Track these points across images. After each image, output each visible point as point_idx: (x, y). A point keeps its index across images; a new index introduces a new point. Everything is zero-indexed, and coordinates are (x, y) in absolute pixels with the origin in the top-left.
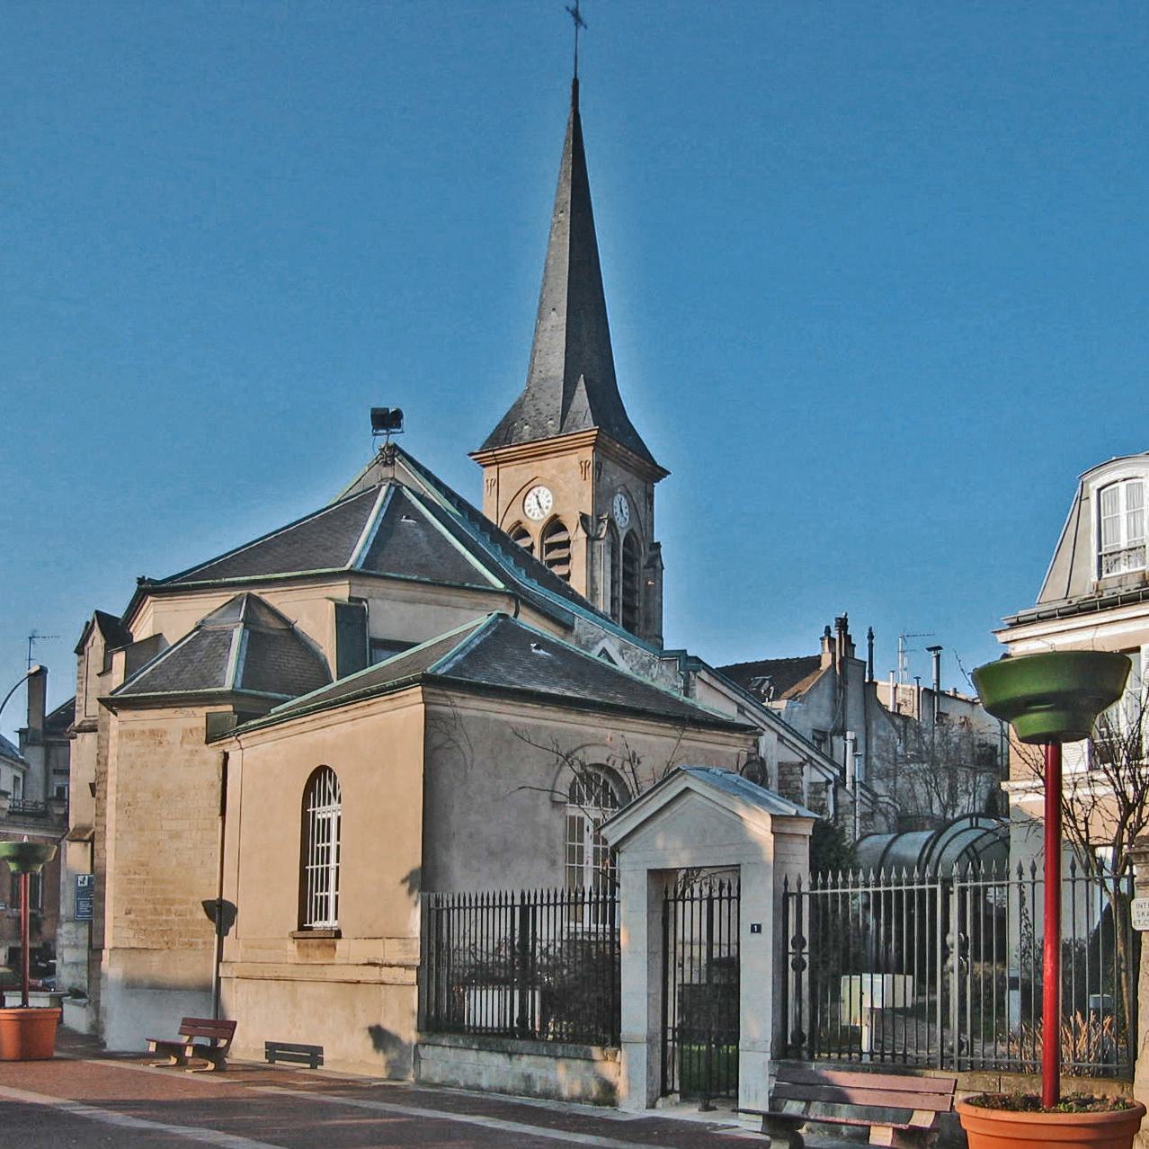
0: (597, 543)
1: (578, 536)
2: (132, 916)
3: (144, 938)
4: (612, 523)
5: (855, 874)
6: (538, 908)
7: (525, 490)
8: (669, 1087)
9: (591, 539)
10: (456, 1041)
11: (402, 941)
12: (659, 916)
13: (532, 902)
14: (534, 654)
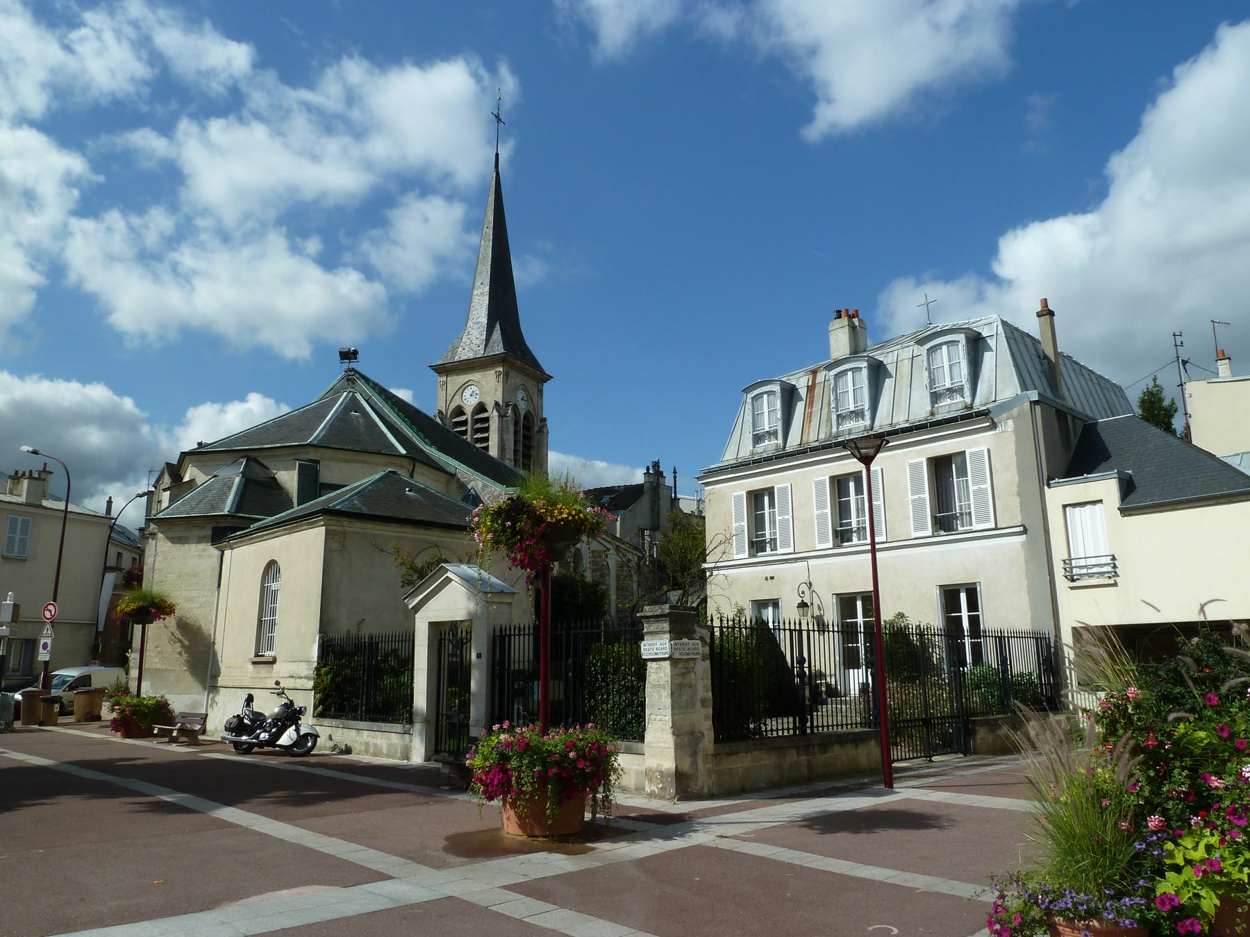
1: (494, 416)
4: (515, 408)
7: (464, 387)
9: (501, 416)
12: (436, 648)
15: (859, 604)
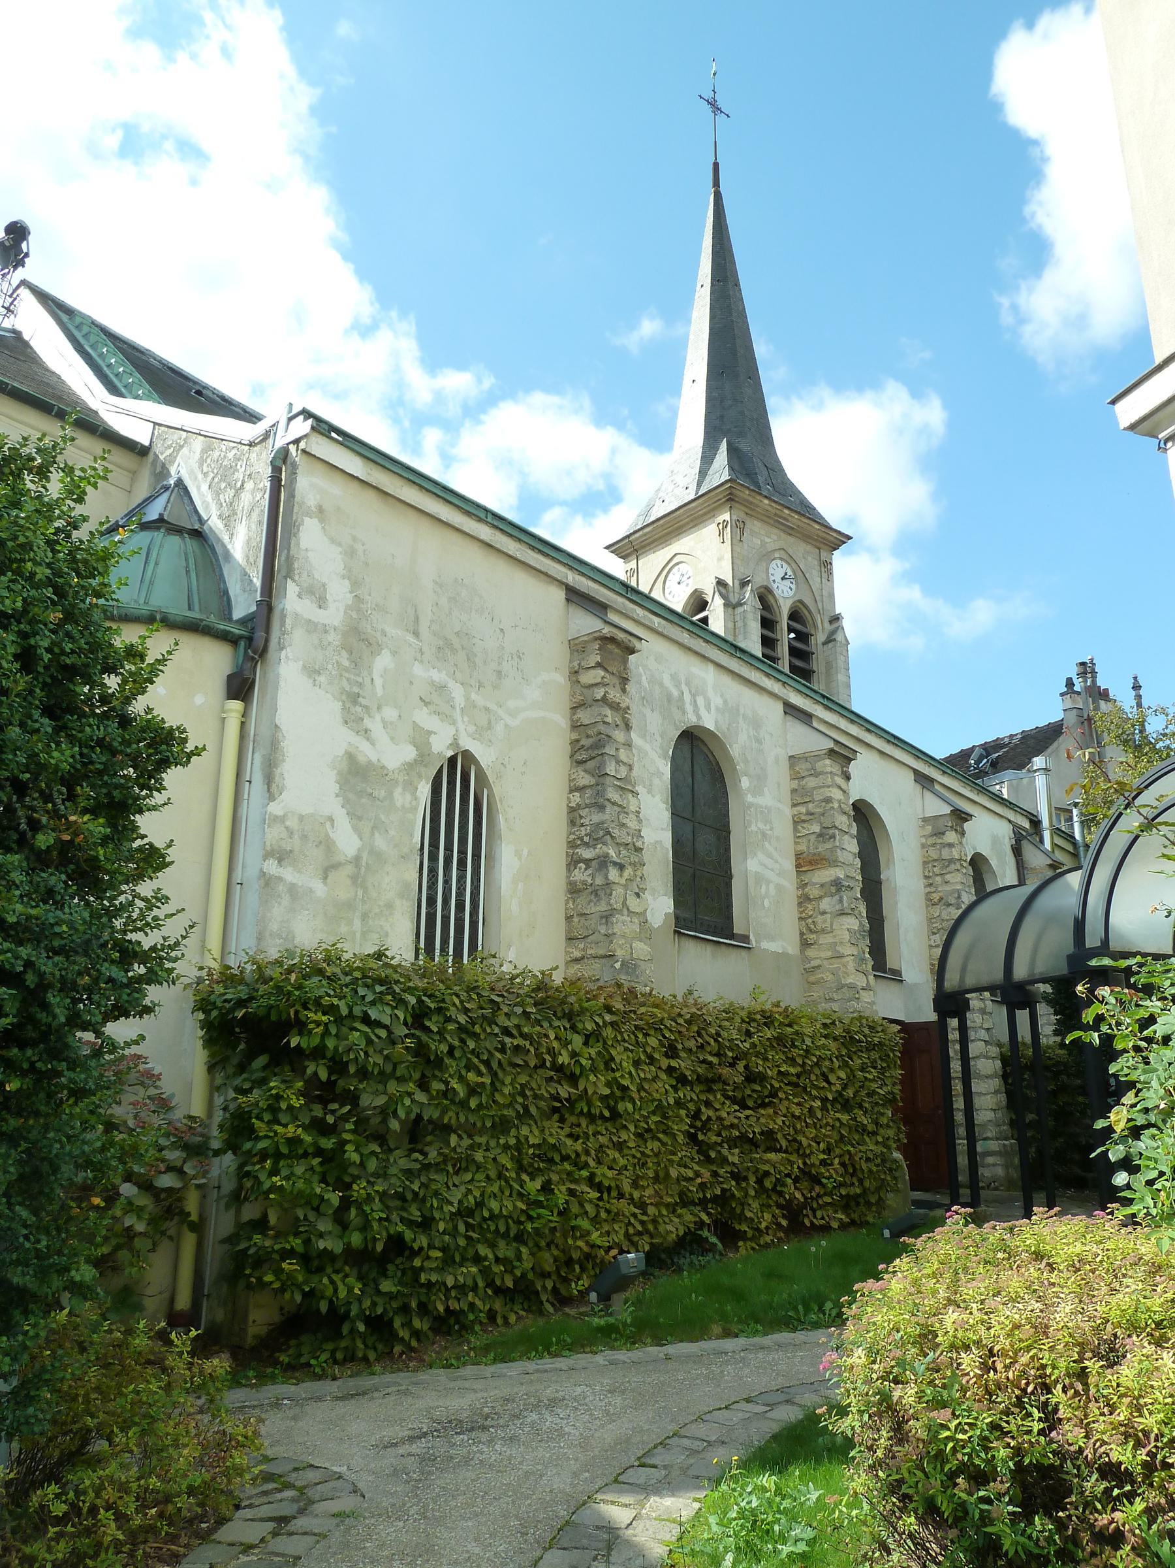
0: (740, 610)
4: (765, 598)
15: (993, 1168)
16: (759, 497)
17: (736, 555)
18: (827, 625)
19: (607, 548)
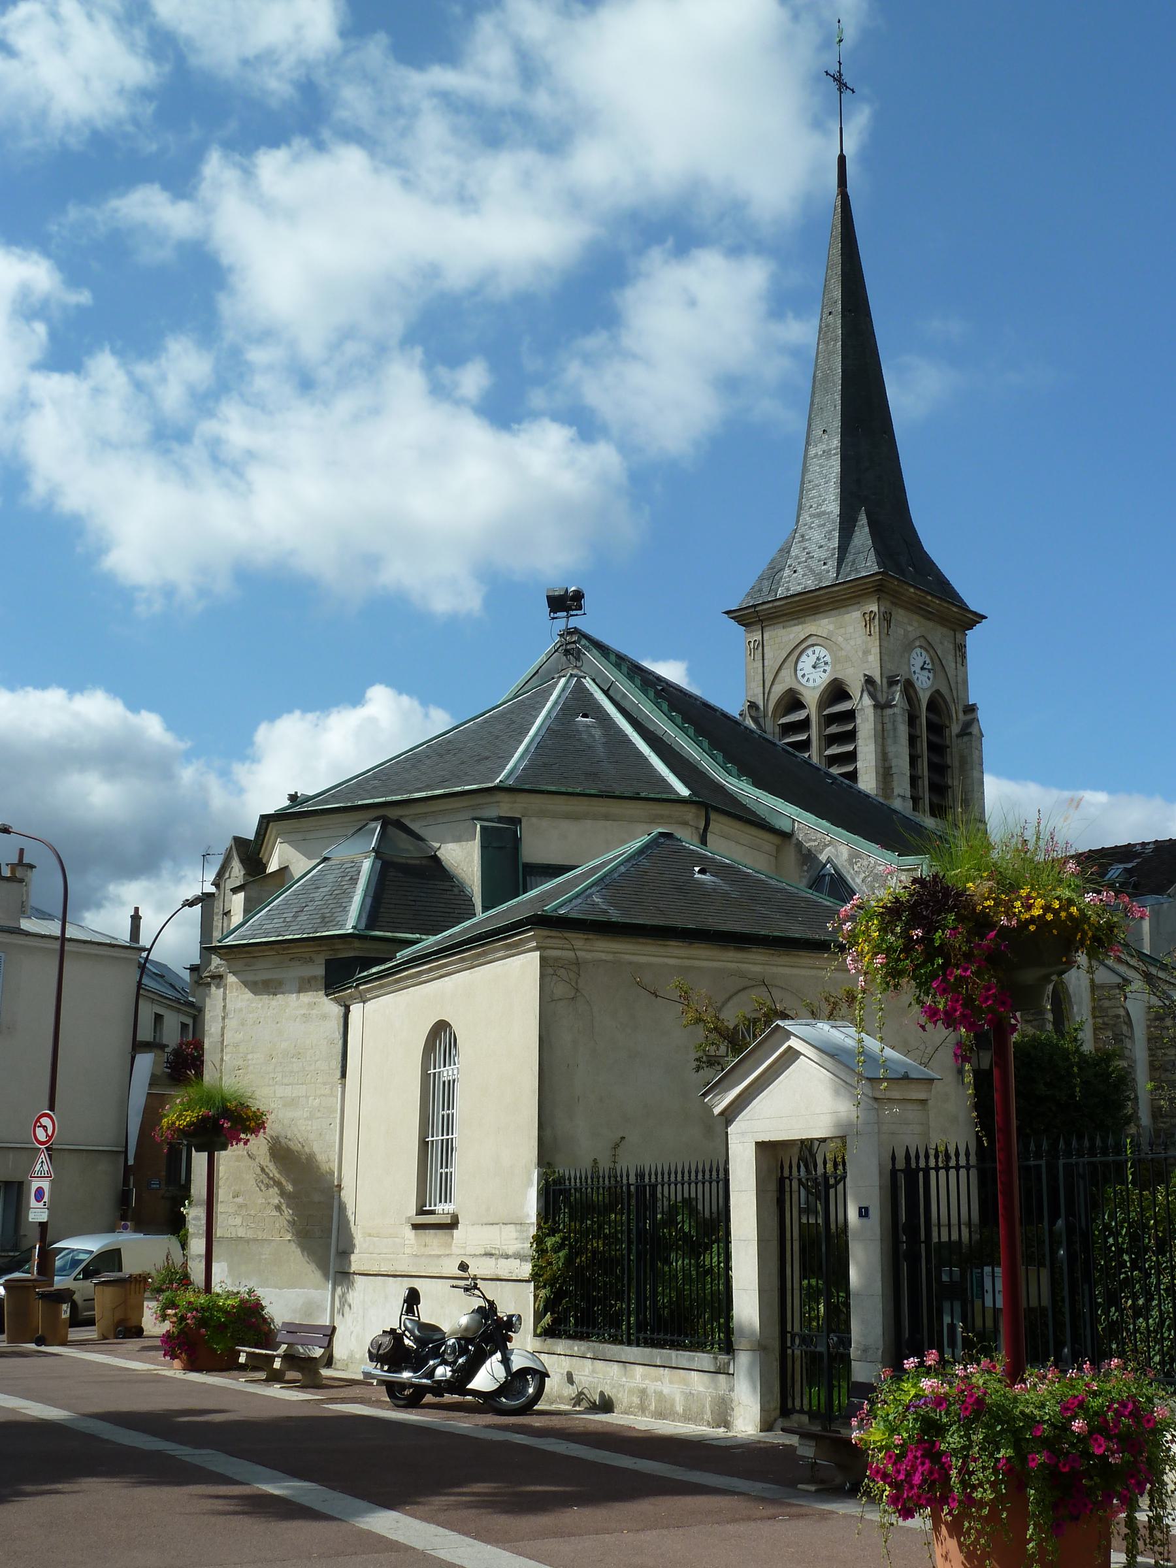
0: (889, 711)
1: (864, 705)
2: (240, 1200)
3: (253, 1225)
4: (909, 686)
5: (1080, 1137)
6: (933, 1173)
7: (798, 650)
8: (790, 1405)
9: (879, 707)
10: (571, 1348)
11: (518, 1227)
13: (922, 1164)
14: (696, 880)
16: (906, 587)
17: (885, 658)
18: (961, 715)
19: (727, 613)
